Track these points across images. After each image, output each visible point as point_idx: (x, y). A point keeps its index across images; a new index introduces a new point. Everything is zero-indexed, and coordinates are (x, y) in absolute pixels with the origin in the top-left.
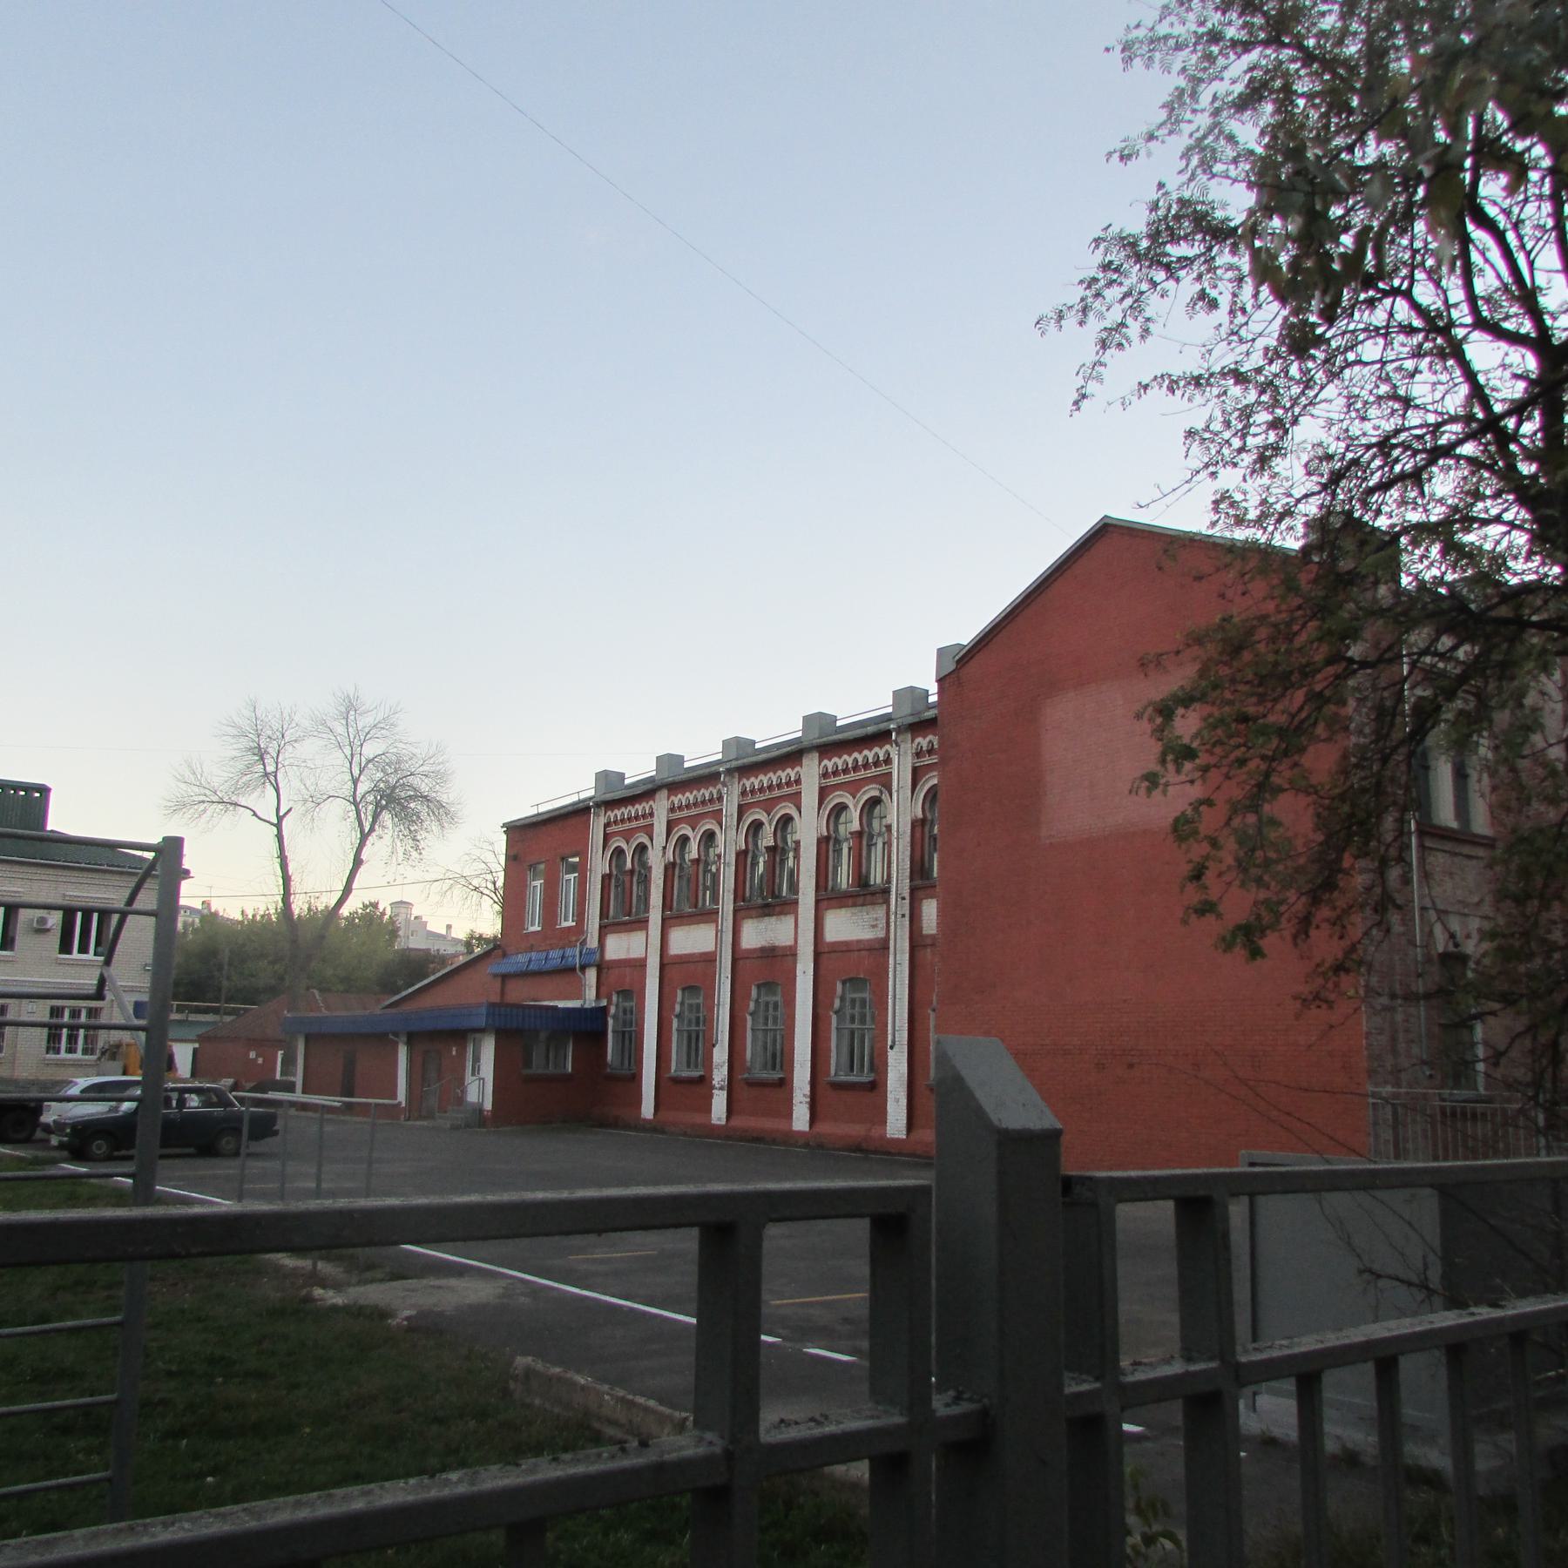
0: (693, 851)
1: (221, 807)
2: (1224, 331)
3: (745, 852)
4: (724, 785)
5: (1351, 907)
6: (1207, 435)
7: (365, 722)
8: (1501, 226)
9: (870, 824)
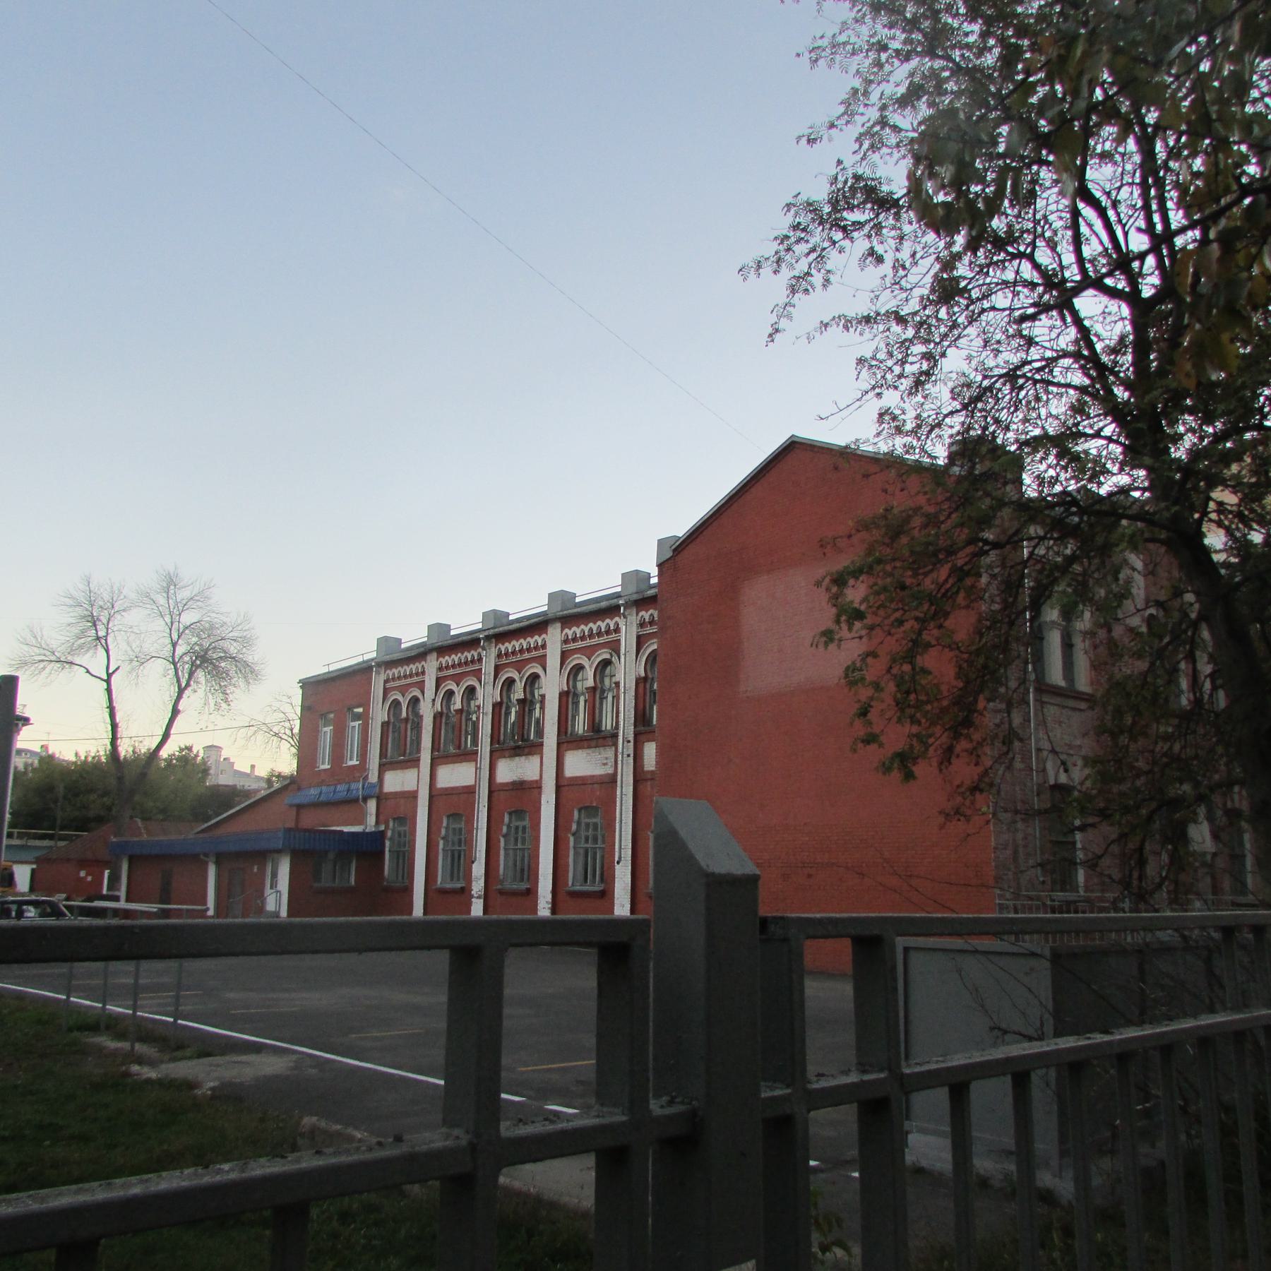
0: (457, 703)
1: (58, 665)
2: (888, 281)
3: (500, 704)
4: (484, 649)
5: (984, 740)
6: (874, 363)
7: (183, 595)
8: (1103, 204)
9: (602, 681)
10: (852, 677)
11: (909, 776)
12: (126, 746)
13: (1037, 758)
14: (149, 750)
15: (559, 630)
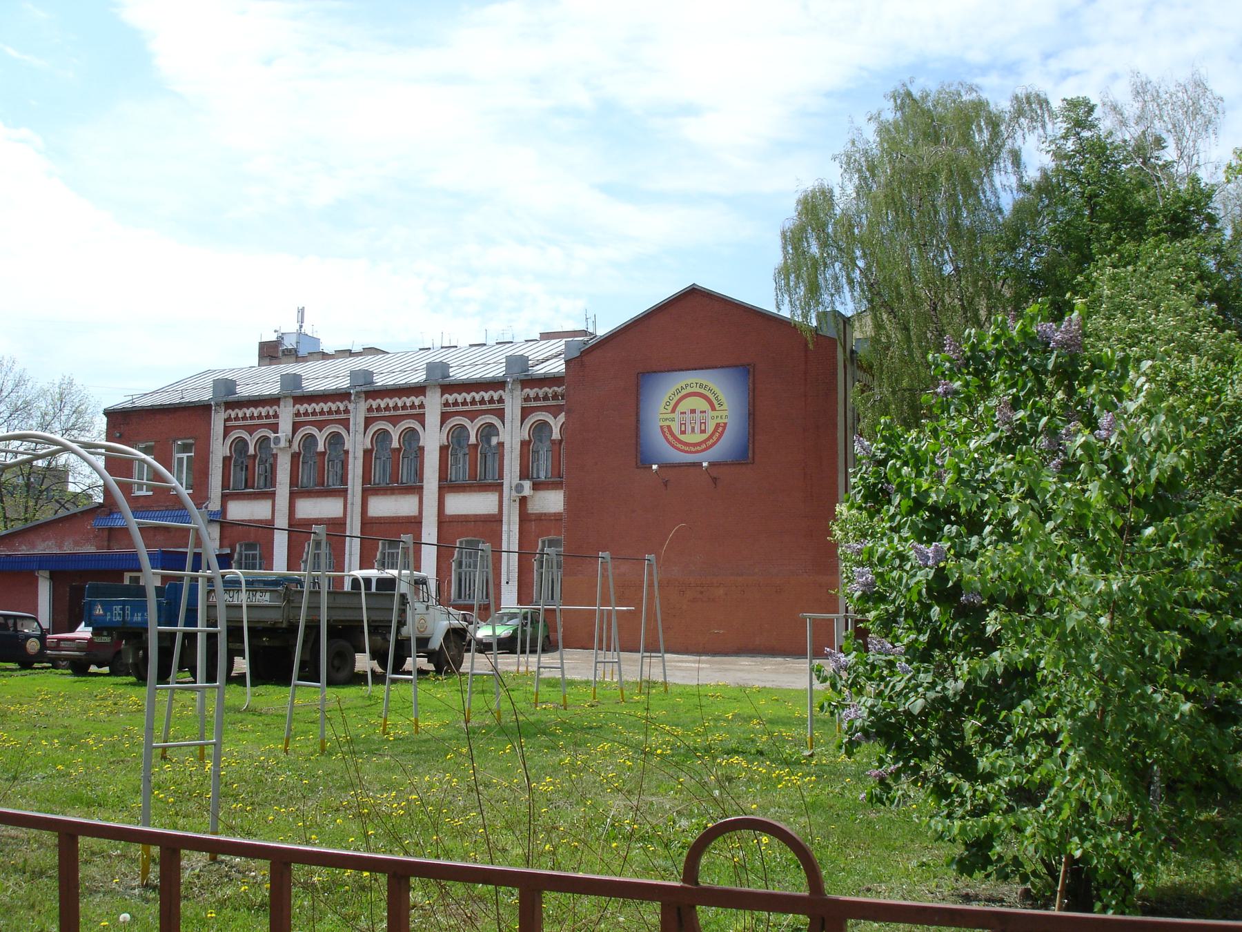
15: (439, 394)
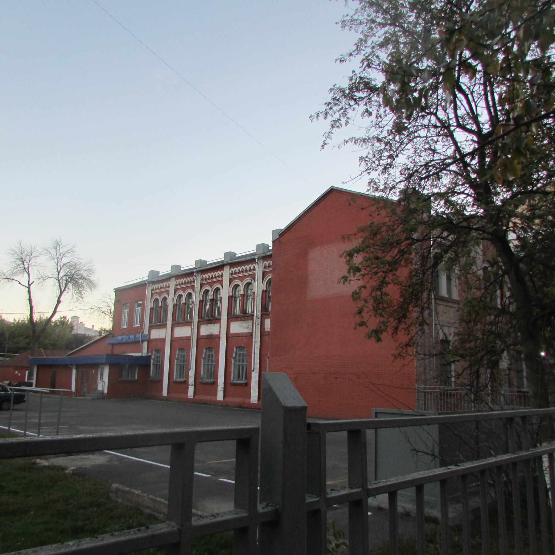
0: (184, 300)
1: (6, 280)
2: (374, 123)
3: (202, 301)
4: (196, 276)
6: (367, 159)
7: (63, 250)
9: (247, 292)
10: (356, 296)
11: (379, 340)
12: (36, 316)
13: (435, 329)
14: (47, 318)
15: (229, 269)
